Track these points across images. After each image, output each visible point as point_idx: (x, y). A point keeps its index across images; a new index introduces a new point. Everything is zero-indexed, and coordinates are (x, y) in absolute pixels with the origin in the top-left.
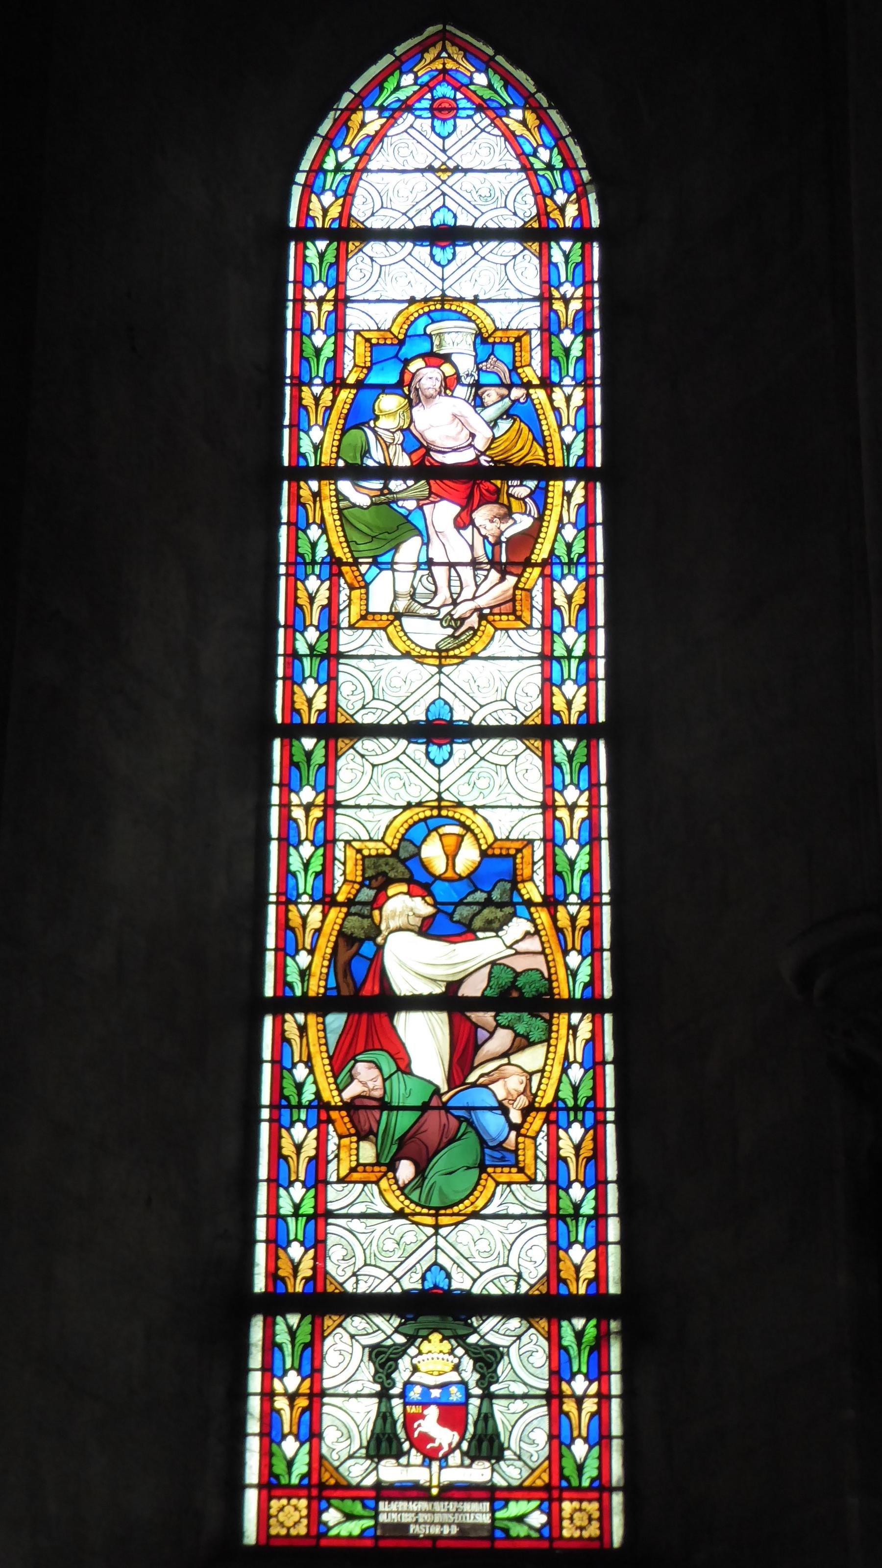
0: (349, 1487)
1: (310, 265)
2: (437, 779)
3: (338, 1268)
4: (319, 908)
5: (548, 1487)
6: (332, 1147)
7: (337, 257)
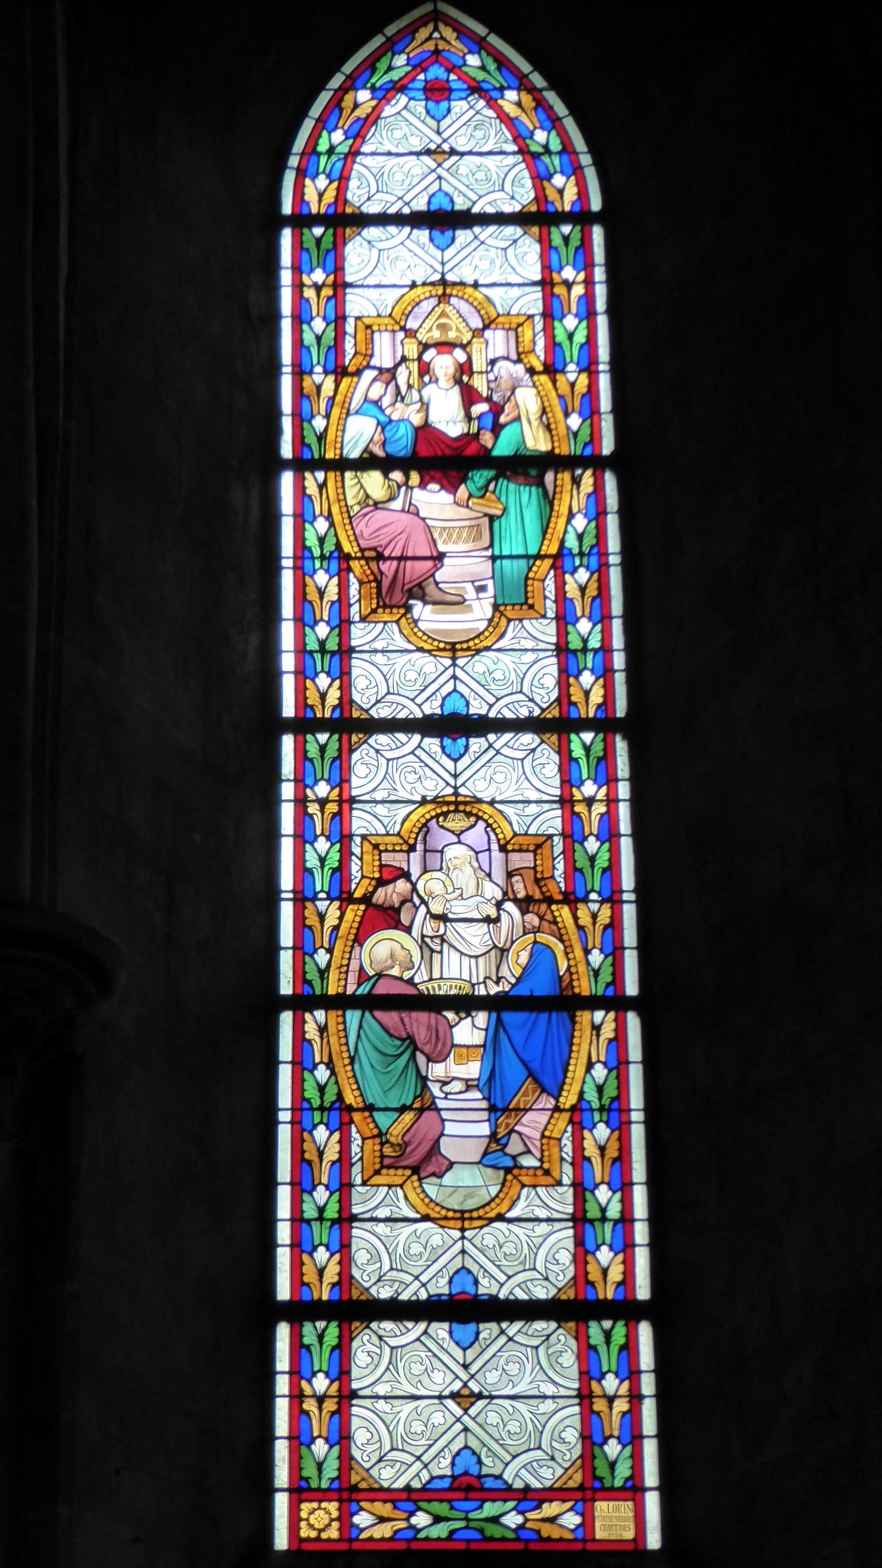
0: (381, 1489)
1: (310, 928)
2: (461, 1362)
3: (364, 1273)
4: (336, 904)
5: (581, 1488)
6: (355, 1149)
7: (335, 243)
